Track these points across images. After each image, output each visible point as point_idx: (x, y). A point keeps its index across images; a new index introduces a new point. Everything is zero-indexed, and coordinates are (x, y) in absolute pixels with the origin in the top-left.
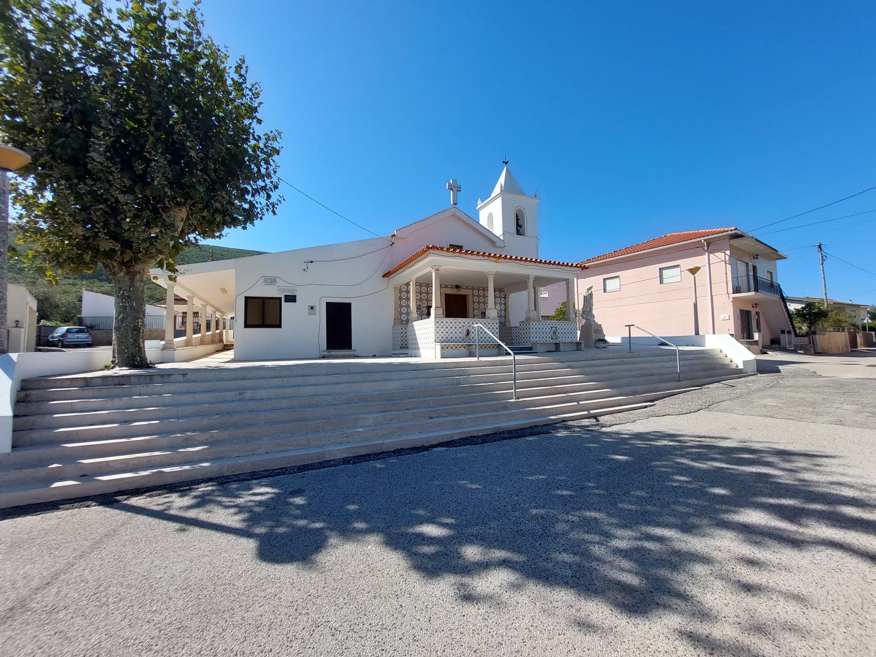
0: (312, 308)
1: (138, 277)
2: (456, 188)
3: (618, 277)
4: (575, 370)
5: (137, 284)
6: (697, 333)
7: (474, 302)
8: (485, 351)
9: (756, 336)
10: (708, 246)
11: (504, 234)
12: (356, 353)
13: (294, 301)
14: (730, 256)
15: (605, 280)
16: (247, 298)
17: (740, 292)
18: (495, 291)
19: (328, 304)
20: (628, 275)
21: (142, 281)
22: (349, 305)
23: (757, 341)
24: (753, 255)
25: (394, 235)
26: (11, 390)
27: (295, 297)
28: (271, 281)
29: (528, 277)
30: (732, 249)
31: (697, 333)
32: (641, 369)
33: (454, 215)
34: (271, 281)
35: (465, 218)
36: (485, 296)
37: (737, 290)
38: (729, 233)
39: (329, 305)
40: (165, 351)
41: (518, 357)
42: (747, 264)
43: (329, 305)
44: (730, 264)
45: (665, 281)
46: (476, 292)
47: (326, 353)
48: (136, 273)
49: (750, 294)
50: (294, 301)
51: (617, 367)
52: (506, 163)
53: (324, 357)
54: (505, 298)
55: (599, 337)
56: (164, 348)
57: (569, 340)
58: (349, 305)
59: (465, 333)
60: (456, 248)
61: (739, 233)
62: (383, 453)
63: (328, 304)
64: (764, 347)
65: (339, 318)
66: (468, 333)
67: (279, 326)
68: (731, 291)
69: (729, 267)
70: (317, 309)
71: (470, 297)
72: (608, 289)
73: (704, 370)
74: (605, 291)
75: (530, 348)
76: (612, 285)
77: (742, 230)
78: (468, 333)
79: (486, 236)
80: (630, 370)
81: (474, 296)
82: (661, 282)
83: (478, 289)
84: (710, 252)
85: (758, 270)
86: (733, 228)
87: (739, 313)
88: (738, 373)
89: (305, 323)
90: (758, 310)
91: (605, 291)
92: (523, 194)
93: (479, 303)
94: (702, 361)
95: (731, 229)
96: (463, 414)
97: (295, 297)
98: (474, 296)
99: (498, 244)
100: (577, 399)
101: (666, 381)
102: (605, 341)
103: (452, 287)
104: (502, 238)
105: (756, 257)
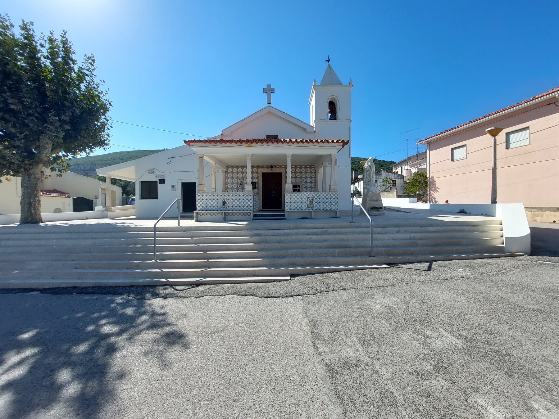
0: (173, 187)
1: (32, 176)
2: (269, 91)
4: (254, 239)
5: (32, 180)
11: (315, 121)
13: (164, 183)
15: (453, 149)
16: (142, 182)
18: (292, 168)
25: (222, 134)
26: (399, 207)
27: (164, 180)
29: (285, 156)
32: (341, 240)
33: (269, 112)
35: (278, 113)
39: (184, 184)
43: (184, 184)
45: (512, 146)
50: (164, 183)
51: (293, 237)
52: (329, 61)
54: (315, 173)
56: (105, 210)
59: (222, 203)
60: (273, 139)
65: (189, 192)
66: (224, 203)
67: (157, 198)
70: (176, 187)
72: (455, 158)
73: (436, 245)
74: (452, 160)
76: (459, 154)
78: (224, 203)
79: (304, 128)
91: (452, 160)
94: (448, 234)
97: (164, 180)
103: (268, 167)
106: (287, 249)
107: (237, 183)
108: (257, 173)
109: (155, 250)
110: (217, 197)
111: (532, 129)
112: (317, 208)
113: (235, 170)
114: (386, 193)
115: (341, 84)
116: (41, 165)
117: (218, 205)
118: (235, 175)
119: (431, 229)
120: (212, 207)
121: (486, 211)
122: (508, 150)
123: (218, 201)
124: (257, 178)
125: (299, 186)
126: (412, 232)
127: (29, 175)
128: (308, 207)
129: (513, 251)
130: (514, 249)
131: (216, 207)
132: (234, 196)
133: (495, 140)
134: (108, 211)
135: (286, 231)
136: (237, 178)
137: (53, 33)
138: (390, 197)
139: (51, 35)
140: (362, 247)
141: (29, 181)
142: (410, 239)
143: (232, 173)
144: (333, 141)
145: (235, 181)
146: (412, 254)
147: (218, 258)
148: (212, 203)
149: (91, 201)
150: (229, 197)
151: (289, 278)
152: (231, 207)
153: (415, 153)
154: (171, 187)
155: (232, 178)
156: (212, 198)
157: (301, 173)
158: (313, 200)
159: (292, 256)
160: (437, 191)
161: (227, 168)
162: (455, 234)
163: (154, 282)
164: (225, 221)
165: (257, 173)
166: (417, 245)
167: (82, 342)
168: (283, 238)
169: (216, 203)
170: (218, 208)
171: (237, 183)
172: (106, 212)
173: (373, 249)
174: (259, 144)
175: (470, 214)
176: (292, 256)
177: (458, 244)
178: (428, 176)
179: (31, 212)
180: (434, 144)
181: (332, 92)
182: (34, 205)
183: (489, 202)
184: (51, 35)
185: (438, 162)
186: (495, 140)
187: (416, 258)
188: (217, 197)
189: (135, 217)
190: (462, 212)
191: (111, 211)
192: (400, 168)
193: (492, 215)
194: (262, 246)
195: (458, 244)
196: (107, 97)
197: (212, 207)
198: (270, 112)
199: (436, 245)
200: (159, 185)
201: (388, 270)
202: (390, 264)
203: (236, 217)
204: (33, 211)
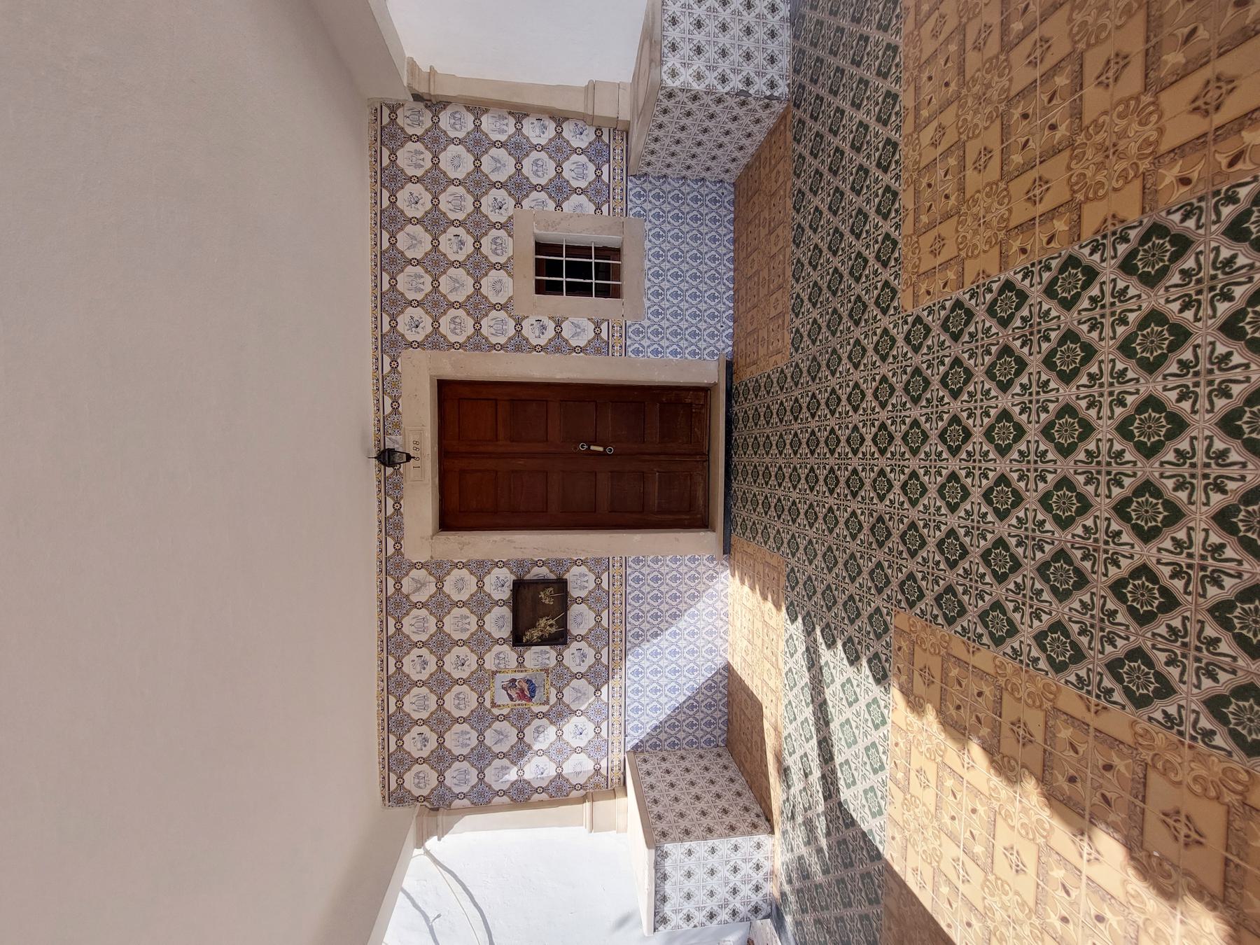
97: (538, 291)
98: (435, 342)
125: (541, 247)
165: (439, 570)
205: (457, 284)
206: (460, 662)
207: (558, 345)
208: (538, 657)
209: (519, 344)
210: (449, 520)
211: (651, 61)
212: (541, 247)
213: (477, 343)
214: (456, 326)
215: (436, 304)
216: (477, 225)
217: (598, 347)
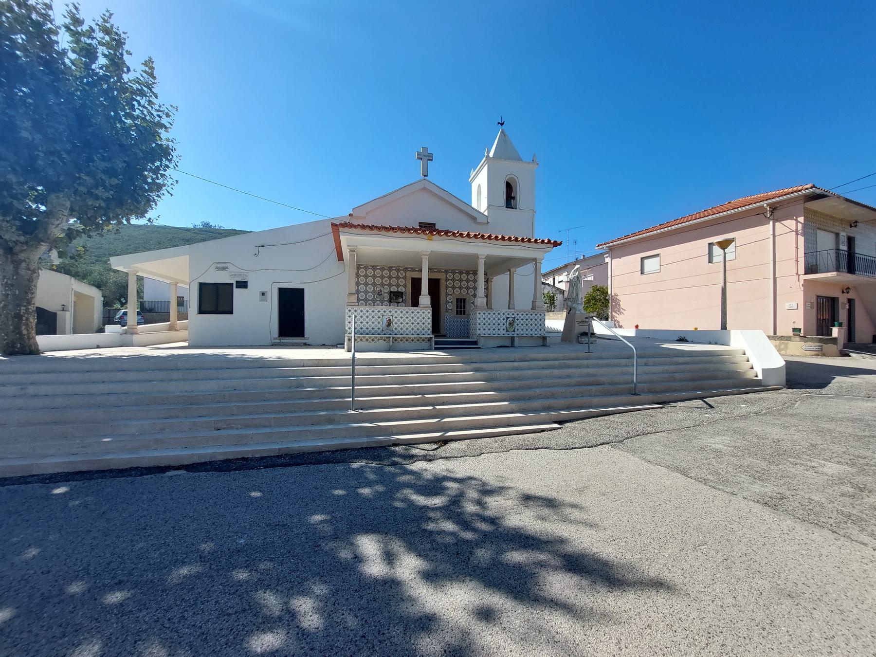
0: (263, 294)
1: (23, 265)
2: (426, 157)
3: (658, 255)
4: (479, 375)
5: (23, 272)
6: (724, 327)
7: (447, 287)
8: (364, 344)
9: (835, 332)
10: (772, 212)
11: (488, 208)
12: (308, 342)
14: (805, 225)
15: (643, 259)
17: (816, 273)
19: (280, 290)
20: (670, 253)
21: (29, 269)
22: (301, 292)
23: (835, 339)
24: (850, 222)
25: (350, 215)
27: (246, 282)
28: (222, 267)
29: (476, 257)
30: (807, 213)
31: (724, 327)
32: (588, 375)
33: (424, 189)
34: (222, 267)
36: (475, 281)
37: (811, 269)
38: (803, 192)
40: (124, 336)
41: (359, 355)
42: (837, 235)
43: (281, 291)
44: (804, 234)
46: (450, 276)
47: (277, 341)
48: (21, 261)
49: (829, 275)
52: (502, 124)
53: (274, 346)
55: (585, 329)
56: (126, 332)
57: (534, 333)
58: (301, 292)
59: (385, 323)
60: (428, 228)
61: (818, 191)
62: (111, 471)
63: (280, 290)
64: (845, 346)
66: (389, 323)
67: (231, 313)
68: (802, 270)
69: (801, 239)
70: (269, 294)
71: (443, 282)
72: (646, 270)
73: (693, 380)
75: (475, 343)
76: (651, 265)
77: (824, 186)
78: (389, 323)
79: (473, 216)
80: (568, 376)
81: (447, 280)
82: (710, 261)
83: (468, 273)
84: (775, 221)
85: (857, 242)
86: (809, 186)
87: (814, 300)
88: (753, 386)
89: (257, 308)
90: (851, 295)
92: (520, 159)
93: (454, 287)
94: (697, 366)
95: (806, 188)
96: (265, 426)
97: (246, 282)
98: (447, 280)
99: (479, 220)
100: (441, 415)
101: (605, 394)
102: (593, 334)
104: (486, 213)
105: (854, 224)
106: (530, 388)
107: (373, 292)
108: (405, 278)
109: (353, 393)
110: (379, 314)
111: (738, 242)
112: (519, 332)
113: (370, 272)
114: (551, 314)
115: (520, 159)
116: (44, 247)
117: (379, 326)
118: (370, 280)
119: (680, 360)
120: (364, 328)
121: (720, 335)
122: (711, 265)
123: (379, 320)
124: (405, 286)
125: (465, 300)
126: (71, 383)
127: (17, 263)
128: (507, 331)
129: (770, 383)
130: (772, 382)
131: (376, 329)
132: (365, 311)
133: (725, 254)
134: (133, 333)
135: (516, 364)
136: (374, 284)
137: (80, 7)
138: (557, 319)
139: (74, 11)
140: (617, 384)
141: (16, 273)
142: (663, 372)
143: (366, 276)
144: (468, 235)
145: (370, 288)
146: (675, 391)
147: (443, 404)
148: (364, 323)
149: (54, 315)
150: (396, 315)
151: (556, 426)
152: (399, 329)
153: (573, 260)
154: (258, 295)
155: (366, 284)
156: (370, 314)
157: (461, 280)
158: (514, 321)
159: (541, 397)
160: (621, 313)
161: (358, 268)
162: (708, 366)
163: (376, 442)
164: (390, 350)
165: (405, 278)
166: (675, 380)
167: (367, 533)
168: (516, 373)
169: (376, 323)
170: (379, 331)
171: (373, 292)
172: (128, 336)
173: (639, 385)
174: (406, 234)
175: (693, 342)
176: (541, 397)
177: (715, 378)
178: (609, 292)
179: (20, 333)
180: (618, 250)
181: (511, 169)
182: (27, 319)
183: (718, 327)
184: (74, 11)
185: (622, 274)
186: (725, 254)
187: (684, 395)
188: (379, 314)
189: (186, 344)
190: (682, 340)
191: (136, 333)
192: (551, 279)
193: (726, 344)
194: (496, 384)
195: (715, 378)
196: (169, 135)
197: (370, 329)
198: (426, 188)
199: (693, 380)
200: (237, 292)
201: (663, 410)
202: (664, 403)
203: (406, 345)
204: (25, 332)
205: (457, 284)
206: (386, 281)
207: (447, 302)
208: (387, 297)
209: (447, 295)
210: (413, 279)
211: (330, 421)
212: (465, 300)
213: (447, 287)
214: (450, 283)
215: (454, 280)
216: (468, 288)
217: (447, 309)
